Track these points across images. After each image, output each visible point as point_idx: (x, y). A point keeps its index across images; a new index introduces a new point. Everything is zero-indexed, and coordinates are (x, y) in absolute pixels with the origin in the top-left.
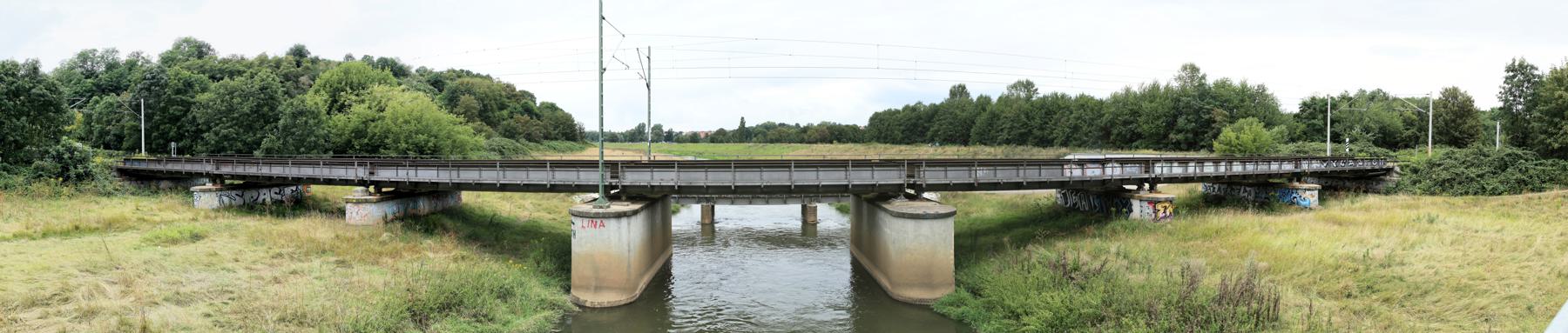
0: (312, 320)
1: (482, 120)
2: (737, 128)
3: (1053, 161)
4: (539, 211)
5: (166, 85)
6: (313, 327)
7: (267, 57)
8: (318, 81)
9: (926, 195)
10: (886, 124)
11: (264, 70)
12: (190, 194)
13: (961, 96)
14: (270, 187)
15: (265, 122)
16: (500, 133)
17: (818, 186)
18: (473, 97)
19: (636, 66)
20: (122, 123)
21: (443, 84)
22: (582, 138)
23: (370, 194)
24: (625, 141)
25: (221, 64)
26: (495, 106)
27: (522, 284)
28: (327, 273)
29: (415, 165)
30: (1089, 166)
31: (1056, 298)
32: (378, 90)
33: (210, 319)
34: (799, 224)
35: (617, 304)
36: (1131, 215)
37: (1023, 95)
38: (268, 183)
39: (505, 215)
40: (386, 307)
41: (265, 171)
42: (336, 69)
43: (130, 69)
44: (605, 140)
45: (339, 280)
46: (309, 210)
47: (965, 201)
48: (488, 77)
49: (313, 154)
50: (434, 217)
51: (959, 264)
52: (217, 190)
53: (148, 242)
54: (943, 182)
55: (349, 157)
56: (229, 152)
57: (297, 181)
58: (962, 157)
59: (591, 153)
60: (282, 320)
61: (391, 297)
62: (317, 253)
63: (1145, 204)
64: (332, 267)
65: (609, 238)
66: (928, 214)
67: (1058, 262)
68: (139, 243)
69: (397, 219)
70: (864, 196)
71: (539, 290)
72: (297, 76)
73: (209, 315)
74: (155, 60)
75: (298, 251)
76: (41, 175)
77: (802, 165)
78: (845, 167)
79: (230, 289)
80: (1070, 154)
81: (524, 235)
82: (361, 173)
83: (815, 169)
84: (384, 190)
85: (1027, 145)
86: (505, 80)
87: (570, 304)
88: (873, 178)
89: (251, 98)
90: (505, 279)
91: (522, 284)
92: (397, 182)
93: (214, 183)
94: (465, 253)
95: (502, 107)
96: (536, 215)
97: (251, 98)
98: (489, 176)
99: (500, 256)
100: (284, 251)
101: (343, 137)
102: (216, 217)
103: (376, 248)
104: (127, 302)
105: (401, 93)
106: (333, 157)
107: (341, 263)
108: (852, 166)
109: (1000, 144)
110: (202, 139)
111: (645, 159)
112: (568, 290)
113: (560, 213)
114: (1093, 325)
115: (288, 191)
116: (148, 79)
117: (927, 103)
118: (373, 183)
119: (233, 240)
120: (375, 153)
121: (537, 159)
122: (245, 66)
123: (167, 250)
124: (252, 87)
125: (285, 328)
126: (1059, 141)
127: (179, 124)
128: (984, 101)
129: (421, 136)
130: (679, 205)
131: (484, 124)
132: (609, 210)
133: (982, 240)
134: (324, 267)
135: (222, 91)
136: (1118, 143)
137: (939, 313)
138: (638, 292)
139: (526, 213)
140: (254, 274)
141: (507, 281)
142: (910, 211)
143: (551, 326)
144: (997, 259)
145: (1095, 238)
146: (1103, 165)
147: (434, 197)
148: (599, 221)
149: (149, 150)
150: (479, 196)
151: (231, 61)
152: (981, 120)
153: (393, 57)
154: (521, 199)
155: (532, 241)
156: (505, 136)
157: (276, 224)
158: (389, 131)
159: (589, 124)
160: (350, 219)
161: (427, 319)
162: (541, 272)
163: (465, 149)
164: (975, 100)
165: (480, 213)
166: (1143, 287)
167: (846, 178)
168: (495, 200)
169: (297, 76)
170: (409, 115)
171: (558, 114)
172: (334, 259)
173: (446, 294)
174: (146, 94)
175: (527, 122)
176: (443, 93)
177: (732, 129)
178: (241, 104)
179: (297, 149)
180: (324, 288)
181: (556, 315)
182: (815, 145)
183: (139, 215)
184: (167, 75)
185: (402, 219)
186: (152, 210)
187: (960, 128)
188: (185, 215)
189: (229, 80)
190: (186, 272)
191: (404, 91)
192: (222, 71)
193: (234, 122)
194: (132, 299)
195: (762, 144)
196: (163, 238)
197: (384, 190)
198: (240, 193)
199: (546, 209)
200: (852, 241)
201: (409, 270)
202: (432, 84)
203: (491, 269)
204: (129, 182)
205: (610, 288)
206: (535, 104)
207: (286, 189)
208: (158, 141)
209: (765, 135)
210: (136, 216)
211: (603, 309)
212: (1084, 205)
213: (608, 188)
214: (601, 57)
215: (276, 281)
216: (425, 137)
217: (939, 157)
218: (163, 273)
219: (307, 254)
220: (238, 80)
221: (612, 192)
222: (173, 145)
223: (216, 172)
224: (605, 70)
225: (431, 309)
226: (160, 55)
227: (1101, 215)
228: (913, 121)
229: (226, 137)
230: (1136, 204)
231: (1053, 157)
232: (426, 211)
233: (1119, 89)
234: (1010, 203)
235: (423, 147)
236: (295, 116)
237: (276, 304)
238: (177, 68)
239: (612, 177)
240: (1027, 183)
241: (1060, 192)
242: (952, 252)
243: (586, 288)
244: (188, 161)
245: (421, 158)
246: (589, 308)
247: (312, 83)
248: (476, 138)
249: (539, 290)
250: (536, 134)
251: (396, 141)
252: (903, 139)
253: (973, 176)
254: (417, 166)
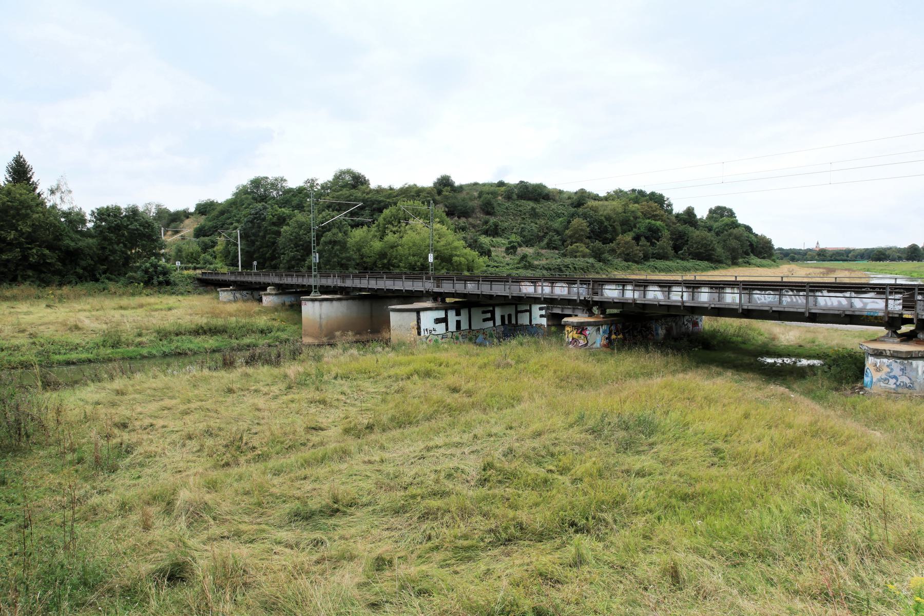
12: (218, 292)
76: (132, 282)
84: (608, 311)
93: (435, 300)
118: (596, 303)
197: (608, 311)
223: (436, 290)
245: (414, 274)
253: (507, 290)
254: (491, 281)
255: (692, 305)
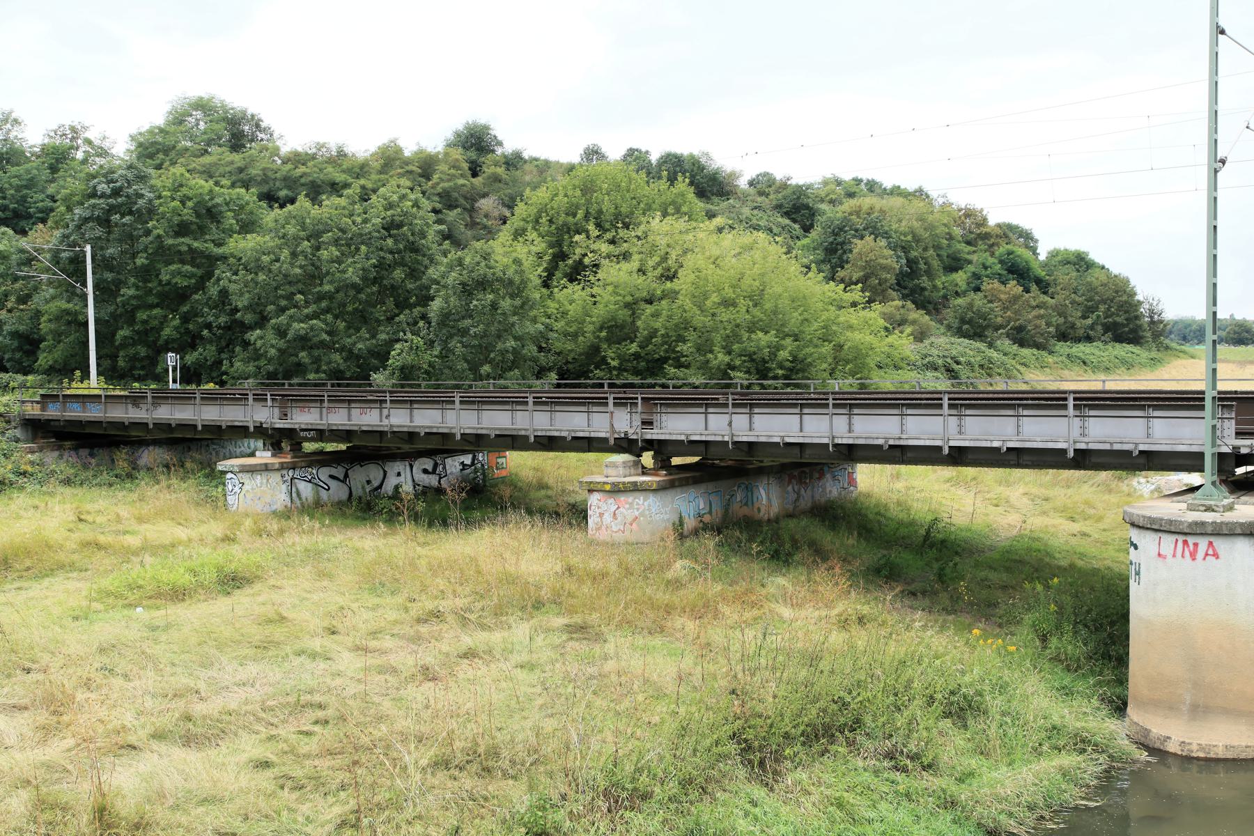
0: (513, 762)
1: (904, 297)
4: (1044, 513)
5: (151, 211)
6: (514, 778)
7: (399, 151)
8: (520, 209)
11: (393, 182)
12: (216, 477)
14: (410, 457)
15: (397, 306)
16: (949, 327)
18: (883, 243)
20: (33, 304)
21: (812, 213)
22: (1157, 335)
23: (645, 471)
25: (289, 166)
26: (935, 263)
27: (1003, 688)
28: (545, 655)
29: (749, 403)
32: (660, 228)
33: (269, 773)
38: (406, 448)
39: (960, 520)
40: (683, 731)
41: (399, 419)
42: (563, 181)
43: (54, 169)
44: (1221, 340)
45: (573, 669)
46: (503, 508)
48: (920, 194)
49: (512, 380)
50: (792, 523)
52: (283, 467)
53: (111, 600)
55: (594, 386)
56: (311, 376)
57: (476, 442)
60: (442, 764)
61: (694, 709)
62: (523, 608)
64: (557, 639)
68: (85, 603)
69: (706, 527)
71: (1045, 703)
72: (472, 198)
73: (266, 764)
74: (121, 148)
75: (479, 605)
79: (317, 698)
81: (1008, 570)
82: (624, 422)
86: (961, 199)
89: (363, 248)
90: (963, 673)
91: (1003, 688)
92: (706, 443)
93: (276, 448)
95: (954, 264)
96: (1037, 523)
97: (363, 248)
99: (951, 618)
100: (445, 605)
101: (581, 338)
102: (282, 532)
103: (660, 595)
104: (56, 750)
105: (715, 237)
106: (558, 386)
107: (579, 630)
110: (246, 344)
112: (1120, 708)
113: (1100, 519)
115: (453, 465)
116: (103, 196)
118: (650, 444)
119: (325, 583)
120: (653, 375)
122: (348, 171)
123: (159, 615)
124: (365, 221)
125: (449, 784)
127: (185, 309)
129: (760, 334)
131: (909, 304)
132: (1229, 517)
134: (539, 641)
135: (291, 230)
139: (1013, 519)
140: (373, 661)
141: (967, 679)
143: (1076, 791)
147: (791, 477)
148: (1203, 543)
149: (110, 373)
150: (898, 476)
151: (313, 157)
153: (696, 153)
155: (1027, 585)
156: (961, 333)
157: (425, 544)
158: (686, 325)
160: (598, 529)
161: (777, 760)
163: (864, 365)
169: (472, 198)
170: (733, 286)
171: (1093, 277)
172: (560, 621)
173: (821, 704)
174: (99, 232)
175: (1016, 299)
176: (814, 234)
178: (339, 261)
179: (474, 368)
180: (539, 689)
181: (1090, 768)
183: (86, 533)
184: (152, 188)
186: (119, 519)
188: (203, 529)
189: (308, 204)
190: (206, 664)
191: (720, 230)
192: (291, 182)
193: (324, 304)
194: (70, 742)
196: (150, 588)
197: (676, 461)
198: (339, 472)
199: (1062, 510)
201: (735, 647)
202: (787, 214)
203: (929, 647)
204: (56, 454)
205: (1231, 712)
206: (1035, 253)
207: (449, 461)
208: (132, 351)
210: (76, 536)
211: (1210, 763)
215: (427, 674)
216: (771, 337)
218: (151, 674)
219: (499, 611)
220: (331, 204)
221: (1240, 471)
222: (171, 359)
224: (1223, 162)
225: (786, 736)
226: (133, 138)
229: (303, 341)
232: (775, 509)
235: (764, 361)
236: (467, 290)
237: (425, 729)
238: (178, 170)
239: (1239, 434)
243: (1170, 707)
244: (209, 398)
245: (763, 387)
246: (1175, 755)
247: (508, 214)
248: (891, 339)
251: (704, 348)
254: (752, 406)
255: (851, 442)
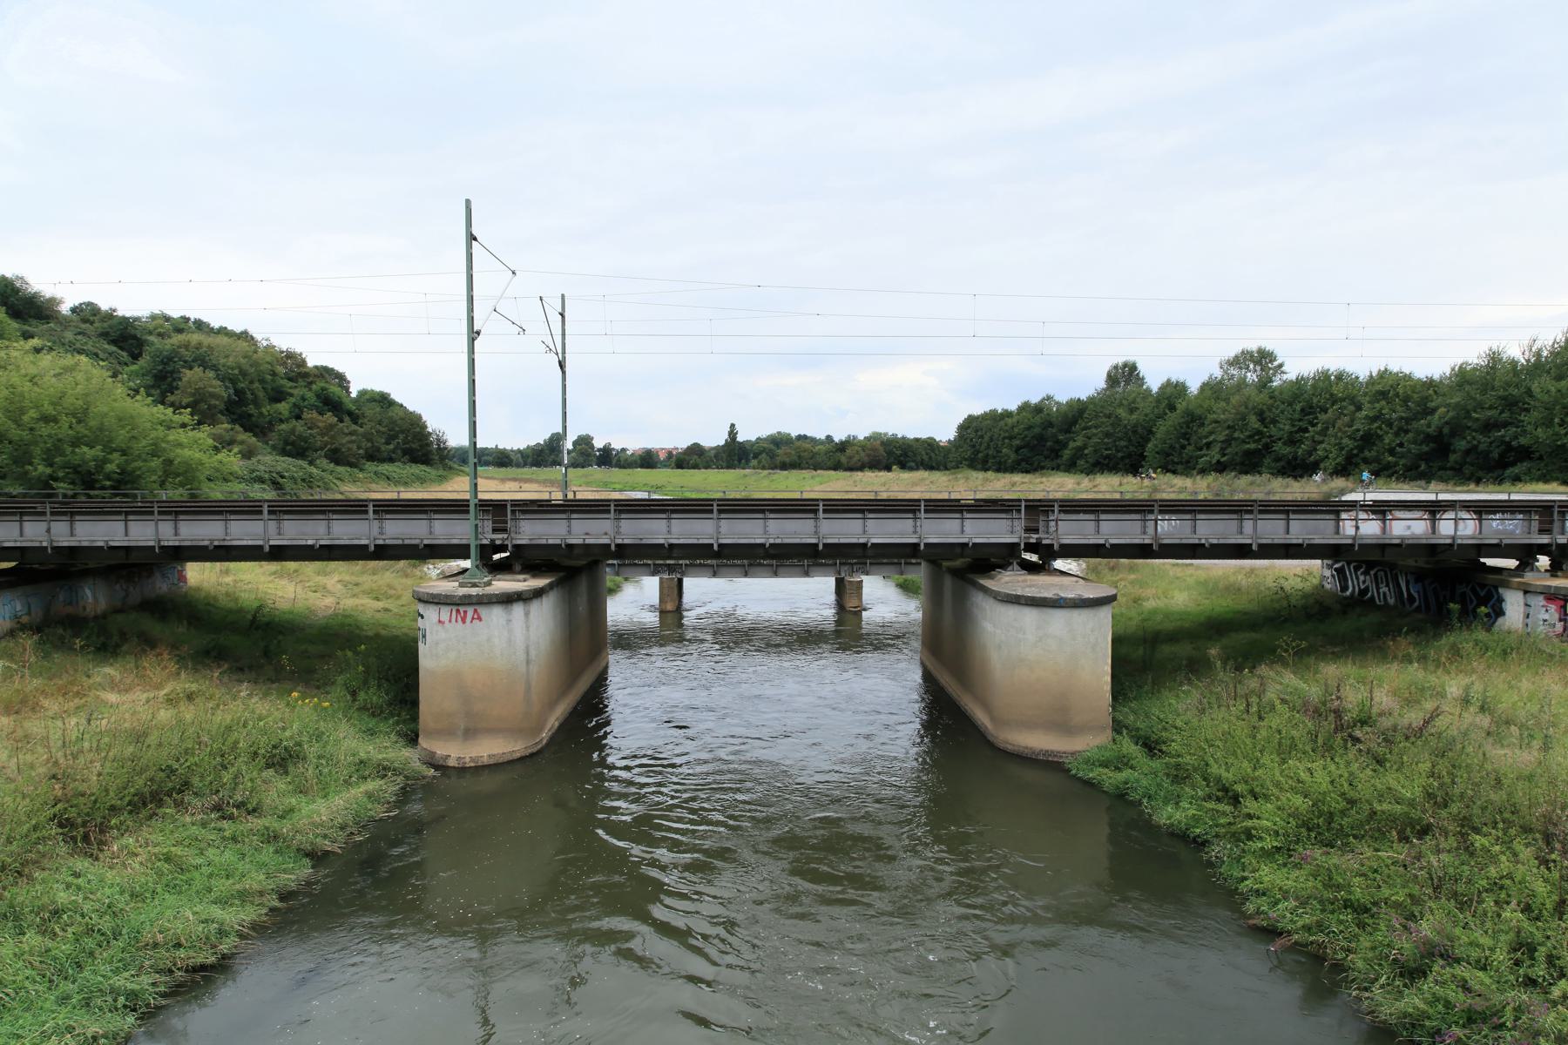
1: (233, 422)
2: (722, 443)
3: (1316, 503)
9: (1059, 564)
10: (987, 438)
13: (1127, 382)
16: (274, 448)
17: (865, 545)
18: (211, 374)
19: (537, 328)
24: (525, 465)
26: (261, 394)
29: (69, 510)
30: (1399, 514)
31: (1320, 774)
34: (829, 613)
35: (506, 758)
36: (1500, 620)
37: (1251, 377)
39: (283, 605)
47: (1132, 577)
50: (120, 618)
51: (1119, 692)
54: (1091, 542)
58: (1128, 496)
59: (456, 488)
63: (1539, 601)
65: (489, 640)
66: (1065, 599)
67: (1324, 703)
70: (946, 564)
71: (354, 744)
77: (838, 508)
78: (914, 512)
80: (1352, 491)
83: (860, 516)
85: (1260, 473)
86: (283, 343)
87: (417, 765)
88: (963, 532)
90: (284, 729)
94: (194, 687)
95: (278, 396)
96: (349, 603)
98: (244, 532)
105: (31, 357)
108: (926, 511)
109: (1203, 472)
111: (557, 496)
112: (412, 739)
113: (399, 597)
114: (1404, 839)
117: (1063, 397)
121: (353, 497)
126: (1330, 464)
128: (1173, 391)
129: (85, 449)
130: (618, 579)
131: (237, 427)
132: (489, 590)
133: (1166, 650)
136: (1467, 470)
137: (1080, 779)
138: (545, 735)
139: (329, 601)
141: (288, 733)
142: (1029, 592)
144: (1197, 687)
145: (1411, 662)
146: (1433, 513)
152: (1164, 429)
154: (319, 574)
155: (339, 653)
156: (284, 453)
159: (456, 438)
162: (358, 709)
164: (1155, 389)
165: (232, 605)
166: (1530, 778)
167: (915, 532)
168: (263, 579)
170: (53, 404)
177: (714, 444)
181: (388, 788)
182: (859, 473)
185: (37, 629)
187: (1123, 443)
195: (766, 472)
200: (924, 643)
202: (114, 342)
203: (253, 712)
206: (348, 393)
209: (772, 455)
211: (479, 769)
212: (1384, 593)
213: (486, 551)
214: (471, 309)
217: (1084, 496)
221: (496, 557)
224: (478, 333)
225: (113, 808)
227: (1420, 616)
228: (1037, 430)
230: (1514, 604)
231: (1315, 497)
232: (103, 605)
233: (1473, 354)
234: (1221, 585)
239: (495, 530)
240: (1260, 546)
241: (1330, 567)
242: (1108, 669)
243: (447, 733)
245: (89, 496)
246: (454, 767)
248: (219, 456)
249: (354, 744)
250: (349, 449)
252: (1018, 463)
253: (1151, 530)
255: (177, 544)
